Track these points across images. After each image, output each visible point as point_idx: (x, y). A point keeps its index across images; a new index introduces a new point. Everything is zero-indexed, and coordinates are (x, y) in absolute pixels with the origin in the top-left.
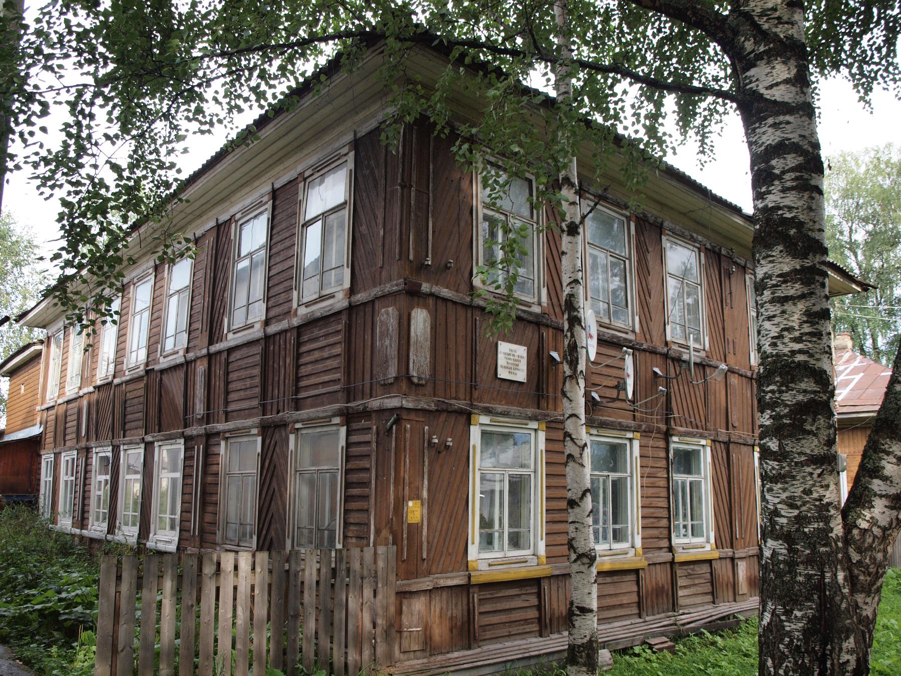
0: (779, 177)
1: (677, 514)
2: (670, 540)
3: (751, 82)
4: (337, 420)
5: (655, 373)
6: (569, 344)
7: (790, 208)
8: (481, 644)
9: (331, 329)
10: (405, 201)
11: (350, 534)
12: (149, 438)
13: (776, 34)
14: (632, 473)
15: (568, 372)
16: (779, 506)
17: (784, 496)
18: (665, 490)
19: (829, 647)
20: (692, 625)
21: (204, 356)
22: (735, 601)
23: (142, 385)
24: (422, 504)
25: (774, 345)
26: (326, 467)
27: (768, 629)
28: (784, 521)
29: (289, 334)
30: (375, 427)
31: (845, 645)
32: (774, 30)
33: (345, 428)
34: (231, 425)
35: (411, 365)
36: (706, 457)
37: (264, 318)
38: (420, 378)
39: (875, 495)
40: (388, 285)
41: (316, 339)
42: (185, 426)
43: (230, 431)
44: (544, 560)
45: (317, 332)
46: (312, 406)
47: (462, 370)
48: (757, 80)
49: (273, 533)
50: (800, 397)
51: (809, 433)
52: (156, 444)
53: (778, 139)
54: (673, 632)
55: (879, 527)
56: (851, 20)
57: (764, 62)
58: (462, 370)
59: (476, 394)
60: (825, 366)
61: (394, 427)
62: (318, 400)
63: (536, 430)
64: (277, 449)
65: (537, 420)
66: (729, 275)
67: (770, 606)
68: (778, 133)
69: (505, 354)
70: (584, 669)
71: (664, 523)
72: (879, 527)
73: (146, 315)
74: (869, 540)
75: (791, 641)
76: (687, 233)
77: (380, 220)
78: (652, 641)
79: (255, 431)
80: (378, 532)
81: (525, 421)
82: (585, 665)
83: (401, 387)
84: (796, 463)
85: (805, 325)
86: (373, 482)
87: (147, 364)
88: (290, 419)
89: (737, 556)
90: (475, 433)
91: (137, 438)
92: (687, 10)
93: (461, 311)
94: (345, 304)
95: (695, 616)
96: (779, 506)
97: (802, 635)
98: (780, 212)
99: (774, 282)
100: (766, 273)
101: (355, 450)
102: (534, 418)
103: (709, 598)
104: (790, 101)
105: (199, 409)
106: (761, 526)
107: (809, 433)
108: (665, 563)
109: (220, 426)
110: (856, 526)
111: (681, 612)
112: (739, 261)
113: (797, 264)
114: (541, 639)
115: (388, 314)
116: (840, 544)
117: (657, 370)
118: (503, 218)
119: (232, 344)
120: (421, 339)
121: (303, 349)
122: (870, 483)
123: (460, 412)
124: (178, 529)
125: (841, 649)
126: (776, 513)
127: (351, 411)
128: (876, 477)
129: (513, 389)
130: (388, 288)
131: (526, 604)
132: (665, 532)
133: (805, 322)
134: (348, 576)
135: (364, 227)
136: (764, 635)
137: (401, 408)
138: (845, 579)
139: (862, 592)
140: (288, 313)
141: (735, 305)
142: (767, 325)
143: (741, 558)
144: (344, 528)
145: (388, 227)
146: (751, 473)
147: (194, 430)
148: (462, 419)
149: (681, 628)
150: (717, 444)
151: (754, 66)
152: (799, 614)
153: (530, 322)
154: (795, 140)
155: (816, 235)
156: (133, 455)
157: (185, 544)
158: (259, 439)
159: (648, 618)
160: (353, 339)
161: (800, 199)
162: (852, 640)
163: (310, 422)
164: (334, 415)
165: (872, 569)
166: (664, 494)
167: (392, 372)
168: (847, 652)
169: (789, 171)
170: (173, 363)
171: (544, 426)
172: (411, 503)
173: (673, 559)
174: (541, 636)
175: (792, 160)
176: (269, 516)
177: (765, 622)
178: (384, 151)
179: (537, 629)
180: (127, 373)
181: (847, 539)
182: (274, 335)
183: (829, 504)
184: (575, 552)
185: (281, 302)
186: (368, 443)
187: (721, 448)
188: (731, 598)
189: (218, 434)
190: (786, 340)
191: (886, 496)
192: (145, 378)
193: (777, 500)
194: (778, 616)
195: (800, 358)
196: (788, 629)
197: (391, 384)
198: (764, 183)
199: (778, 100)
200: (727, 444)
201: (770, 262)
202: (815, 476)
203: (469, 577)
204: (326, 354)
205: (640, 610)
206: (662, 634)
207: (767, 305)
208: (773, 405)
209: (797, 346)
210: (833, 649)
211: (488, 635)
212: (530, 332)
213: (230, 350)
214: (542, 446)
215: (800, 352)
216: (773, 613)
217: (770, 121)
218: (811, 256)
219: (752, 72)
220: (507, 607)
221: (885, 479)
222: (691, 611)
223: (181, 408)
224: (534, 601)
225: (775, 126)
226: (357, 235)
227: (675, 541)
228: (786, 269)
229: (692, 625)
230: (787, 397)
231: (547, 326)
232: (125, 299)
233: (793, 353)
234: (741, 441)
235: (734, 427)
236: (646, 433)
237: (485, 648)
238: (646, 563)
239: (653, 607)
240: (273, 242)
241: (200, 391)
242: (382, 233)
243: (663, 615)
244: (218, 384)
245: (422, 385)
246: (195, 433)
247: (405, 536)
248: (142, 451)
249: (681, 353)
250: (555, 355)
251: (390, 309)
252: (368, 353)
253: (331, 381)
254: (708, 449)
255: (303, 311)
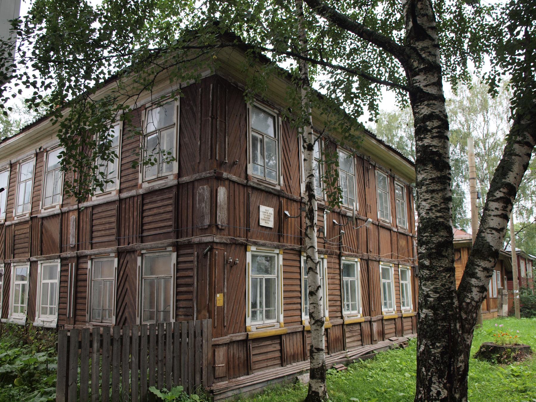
0: (430, 131)
1: (344, 300)
2: (341, 312)
3: (416, 83)
4: (170, 249)
5: (334, 223)
6: (309, 209)
7: (435, 147)
8: (254, 371)
9: (165, 196)
10: (213, 127)
11: (180, 313)
12: (33, 259)
13: (428, 60)
14: (278, 275)
15: (309, 224)
16: (429, 292)
17: (432, 287)
18: (339, 285)
19: (452, 360)
20: (354, 357)
21: (75, 210)
22: (372, 344)
23: (28, 226)
24: (224, 296)
25: (427, 213)
26: (163, 276)
27: (423, 353)
28: (431, 299)
29: (136, 199)
30: (196, 253)
31: (460, 358)
32: (428, 58)
33: (176, 253)
34: (95, 251)
35: (218, 218)
36: (358, 268)
37: (118, 188)
38: (222, 226)
39: (473, 286)
40: (204, 173)
41: (155, 202)
42: (61, 252)
43: (94, 255)
44: (283, 325)
45: (155, 198)
46: (153, 241)
47: (242, 221)
48: (420, 82)
49: (126, 314)
50: (440, 239)
51: (444, 256)
52: (39, 262)
53: (429, 112)
54: (346, 361)
55: (475, 301)
56: (444, 48)
57: (423, 73)
58: (242, 221)
59: (249, 234)
60: (451, 224)
61: (209, 253)
62: (155, 237)
63: (278, 254)
64: (129, 265)
65: (279, 248)
66: (368, 170)
67: (424, 341)
68: (429, 109)
69: (263, 212)
70: (320, 381)
71: (338, 303)
72: (475, 301)
73: (30, 183)
74: (470, 308)
75: (435, 358)
76: (348, 148)
77: (198, 136)
78: (337, 366)
79: (113, 255)
80: (199, 312)
81: (273, 249)
82: (320, 379)
83: (212, 230)
84: (438, 271)
85: (442, 204)
86: (195, 284)
87: (31, 213)
88: (139, 248)
89: (372, 320)
90: (249, 255)
91: (25, 259)
92: (386, 43)
93: (241, 188)
94: (175, 182)
95: (354, 353)
96: (429, 292)
97: (441, 355)
98: (431, 148)
99: (428, 182)
100: (423, 178)
101: (182, 266)
102: (277, 247)
103: (360, 343)
104: (435, 94)
105: (72, 241)
106: (419, 303)
107: (444, 256)
108: (340, 325)
109: (88, 252)
110: (465, 302)
111: (347, 351)
112: (372, 163)
113: (438, 174)
114: (283, 368)
115: (203, 189)
116: (458, 310)
117: (335, 221)
118: (261, 137)
119: (96, 203)
120: (223, 204)
121: (145, 207)
122: (471, 280)
123: (242, 244)
124: (57, 314)
125: (458, 360)
126: (428, 296)
127: (179, 244)
128: (473, 278)
129: (267, 232)
130: (203, 175)
131: (275, 349)
132: (339, 308)
133: (442, 203)
134: (188, 337)
135: (187, 139)
136: (420, 356)
137: (213, 242)
138: (460, 327)
139: (466, 332)
140: (136, 186)
141: (371, 187)
142: (424, 203)
143: (374, 321)
144: (176, 310)
145: (203, 140)
146: (378, 276)
147: (69, 254)
148: (243, 248)
149: (350, 359)
150: (363, 261)
151: (418, 75)
152: (438, 345)
153: (275, 195)
154: (437, 113)
155: (446, 160)
156: (24, 269)
157: (61, 323)
158: (116, 260)
159: (332, 355)
160: (180, 202)
161: (440, 142)
162: (462, 356)
163: (151, 250)
164: (169, 246)
165: (471, 322)
166: (338, 288)
167: (207, 222)
168: (460, 362)
169: (435, 128)
170: (52, 213)
171: (282, 252)
172: (218, 295)
173: (344, 322)
174: (282, 366)
175: (436, 123)
176: (124, 304)
177: (421, 350)
178: (200, 97)
179: (280, 362)
180: (16, 218)
181: (460, 307)
182: (126, 199)
183: (453, 291)
184: (314, 319)
185: (130, 179)
186: (192, 262)
187: (364, 263)
188: (370, 343)
189: (86, 256)
190: (434, 211)
191: (478, 287)
192: (30, 222)
193: (428, 290)
194: (428, 346)
195: (441, 220)
196: (433, 352)
197: (207, 229)
198: (423, 133)
199: (430, 92)
200: (367, 261)
201: (426, 172)
202: (447, 277)
203: (248, 335)
204: (161, 210)
205: (328, 350)
206: (340, 363)
207: (424, 194)
208: (426, 243)
209: (439, 214)
210: (454, 360)
211: (257, 366)
212: (275, 201)
213: (94, 207)
214: (281, 262)
215: (441, 217)
216: (426, 345)
217: (426, 103)
218: (444, 171)
219: (417, 78)
220: (266, 351)
221: (477, 278)
222: (352, 350)
223: (58, 240)
224: (278, 347)
225: (428, 105)
226: (182, 143)
227: (345, 313)
228: (434, 176)
229: (354, 357)
230: (434, 239)
231: (283, 197)
232: (12, 173)
233: (437, 217)
234: (374, 259)
235: (370, 251)
236: (330, 254)
237: (256, 374)
238: (331, 325)
239: (334, 349)
240: (124, 144)
241: (72, 230)
242: (199, 143)
243: (339, 353)
244: (86, 227)
245: (223, 229)
246: (69, 256)
247: (216, 313)
248: (29, 267)
249: (346, 212)
250: (287, 213)
251: (205, 187)
252: (190, 210)
253: (166, 226)
254: (359, 263)
255: (146, 185)
